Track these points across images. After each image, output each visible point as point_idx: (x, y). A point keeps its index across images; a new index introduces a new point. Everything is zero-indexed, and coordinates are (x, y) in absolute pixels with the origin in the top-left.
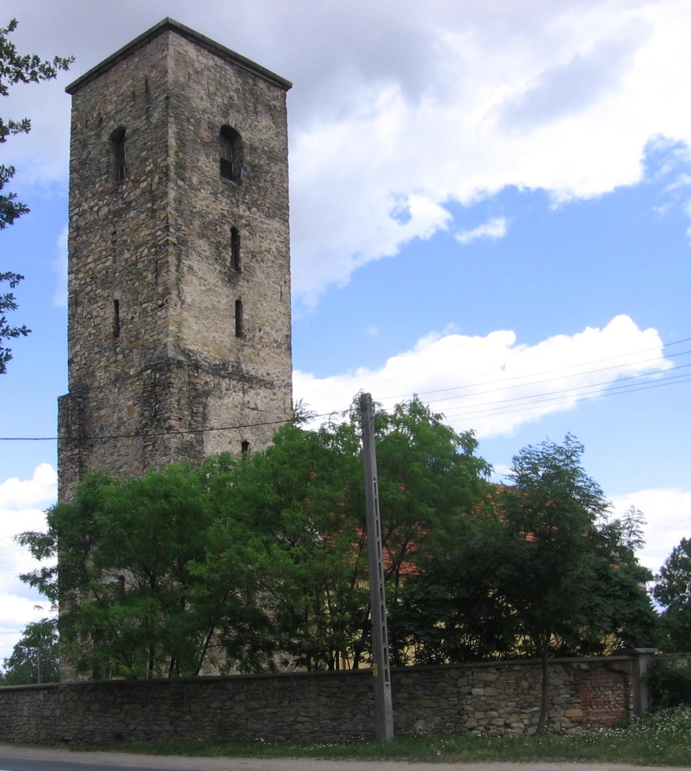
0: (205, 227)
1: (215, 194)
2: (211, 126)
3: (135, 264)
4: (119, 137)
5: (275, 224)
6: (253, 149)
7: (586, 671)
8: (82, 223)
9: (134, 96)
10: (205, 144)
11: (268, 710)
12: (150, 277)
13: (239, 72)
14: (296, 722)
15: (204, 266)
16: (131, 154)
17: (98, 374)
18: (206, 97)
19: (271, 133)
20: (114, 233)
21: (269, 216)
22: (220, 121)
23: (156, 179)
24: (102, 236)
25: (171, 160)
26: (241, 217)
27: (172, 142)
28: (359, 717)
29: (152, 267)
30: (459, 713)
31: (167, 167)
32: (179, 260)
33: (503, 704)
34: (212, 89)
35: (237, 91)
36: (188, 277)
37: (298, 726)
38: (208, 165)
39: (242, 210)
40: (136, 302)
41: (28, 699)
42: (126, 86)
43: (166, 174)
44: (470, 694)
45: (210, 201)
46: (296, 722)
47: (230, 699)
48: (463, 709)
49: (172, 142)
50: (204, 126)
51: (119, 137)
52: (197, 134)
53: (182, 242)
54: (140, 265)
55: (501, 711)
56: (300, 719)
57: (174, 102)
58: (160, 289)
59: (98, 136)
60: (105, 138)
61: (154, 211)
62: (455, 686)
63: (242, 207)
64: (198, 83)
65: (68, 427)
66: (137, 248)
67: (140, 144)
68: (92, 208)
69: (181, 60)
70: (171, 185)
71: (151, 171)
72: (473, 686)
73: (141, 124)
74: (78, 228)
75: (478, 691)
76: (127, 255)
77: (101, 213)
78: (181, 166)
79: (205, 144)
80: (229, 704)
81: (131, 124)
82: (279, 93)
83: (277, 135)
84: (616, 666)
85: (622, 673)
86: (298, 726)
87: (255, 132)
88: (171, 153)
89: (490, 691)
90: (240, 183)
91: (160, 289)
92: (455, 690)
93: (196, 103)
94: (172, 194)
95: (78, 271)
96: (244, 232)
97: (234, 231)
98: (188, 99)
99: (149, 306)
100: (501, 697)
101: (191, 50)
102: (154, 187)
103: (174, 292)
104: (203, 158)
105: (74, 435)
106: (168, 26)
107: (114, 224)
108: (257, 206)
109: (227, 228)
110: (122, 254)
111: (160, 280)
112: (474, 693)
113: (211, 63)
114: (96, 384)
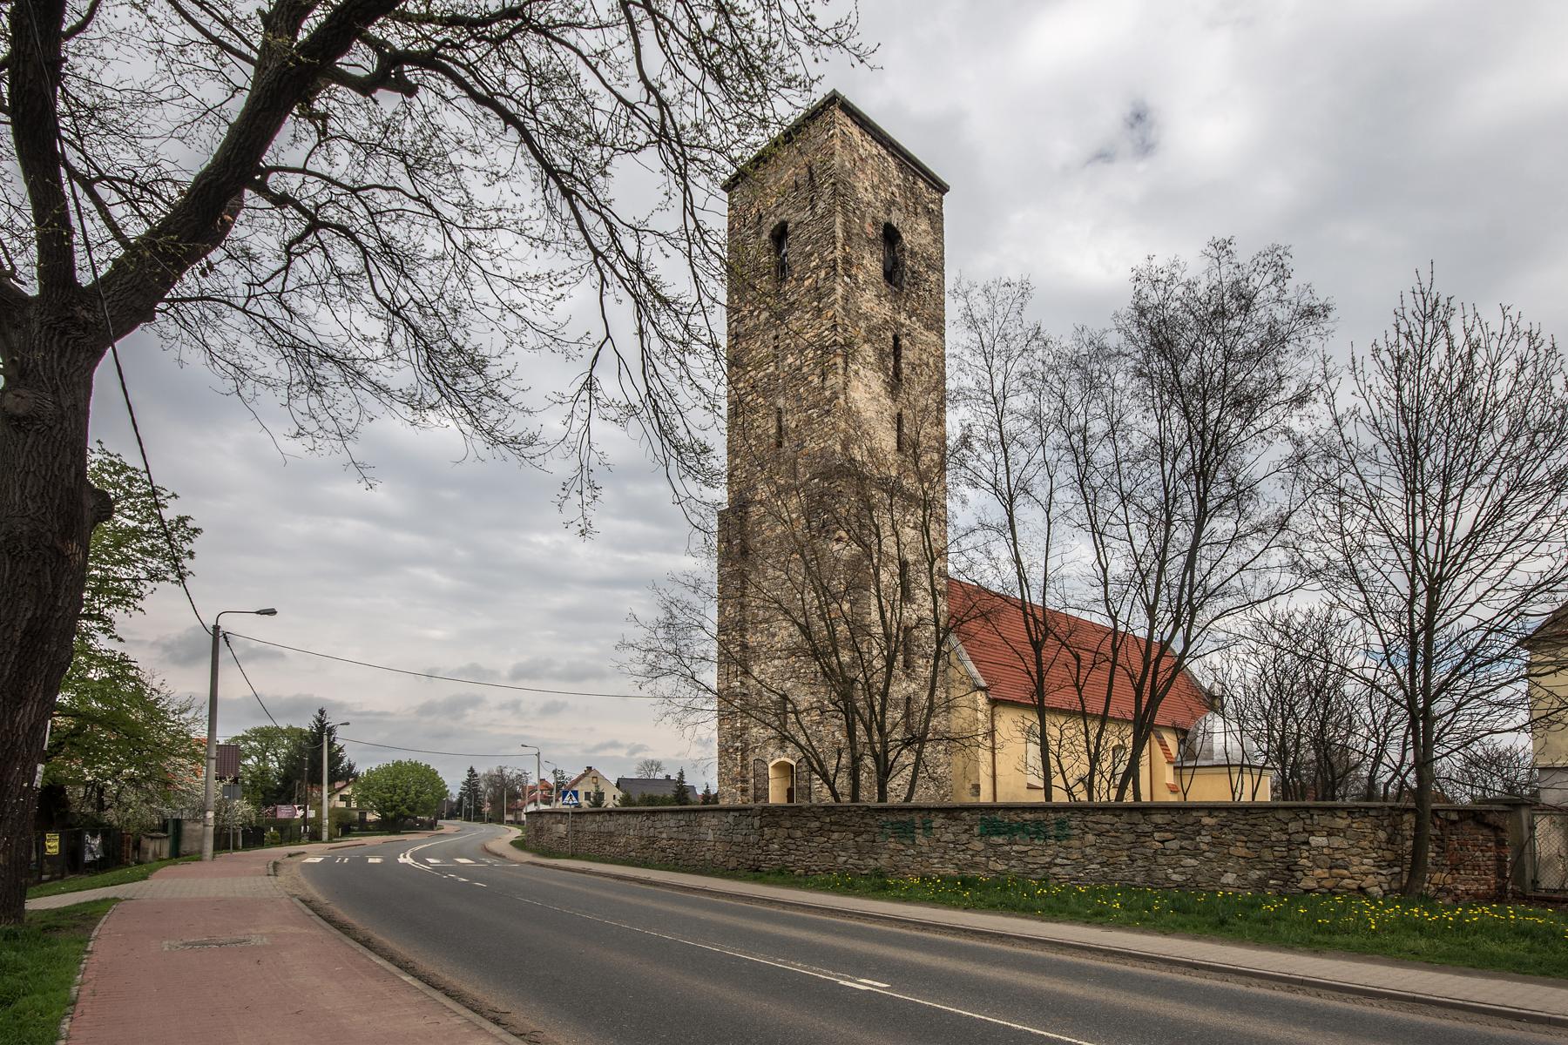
0: (870, 331)
1: (878, 296)
2: (875, 223)
3: (800, 369)
4: (780, 235)
5: (932, 337)
6: (913, 254)
7: (1453, 823)
8: (742, 330)
9: (797, 187)
10: (869, 241)
11: (1015, 848)
12: (816, 381)
13: (901, 167)
14: (1052, 864)
15: (870, 373)
16: (792, 251)
17: (760, 486)
18: (872, 186)
19: (929, 238)
20: (776, 337)
21: (928, 328)
22: (882, 216)
23: (823, 275)
24: (763, 342)
25: (838, 253)
26: (903, 325)
27: (840, 233)
28: (1140, 863)
29: (818, 371)
30: (1288, 869)
31: (835, 260)
32: (846, 363)
33: (1356, 860)
34: (876, 180)
35: (898, 186)
36: (854, 383)
37: (1056, 870)
38: (872, 264)
39: (902, 318)
40: (800, 409)
41: (715, 821)
42: (788, 176)
43: (834, 268)
44: (1307, 843)
45: (873, 304)
46: (1052, 864)
47: (965, 831)
48: (1296, 864)
49: (840, 233)
50: (869, 220)
51: (780, 235)
52: (862, 228)
53: (849, 344)
54: (805, 370)
55: (1355, 869)
56: (1058, 861)
57: (842, 191)
58: (827, 393)
59: (758, 234)
60: (765, 237)
61: (820, 310)
62: (1285, 831)
63: (903, 315)
64: (863, 171)
65: (728, 541)
66: (802, 352)
67: (803, 238)
68: (751, 312)
69: (846, 142)
70: (839, 280)
71: (817, 267)
72: (1312, 833)
73: (806, 215)
74: (737, 336)
75: (1317, 840)
76: (790, 360)
77: (762, 317)
78: (847, 260)
79: (869, 241)
80: (964, 837)
81: (792, 217)
82: (936, 196)
83: (935, 241)
84: (1491, 818)
85: (1496, 829)
86: (1056, 870)
87: (915, 235)
88: (839, 245)
89: (1337, 842)
90: (902, 289)
91: (827, 393)
92: (1284, 837)
93: (861, 194)
94: (840, 290)
95: (738, 380)
96: (905, 342)
97: (896, 339)
98: (854, 188)
99: (814, 413)
100: (1354, 851)
101: (855, 131)
102: (820, 283)
103: (842, 397)
104: (868, 256)
105: (736, 550)
106: (834, 100)
107: (776, 327)
108: (917, 315)
109: (889, 334)
110: (785, 358)
111: (828, 383)
112: (1313, 843)
113: (874, 152)
114: (758, 498)
